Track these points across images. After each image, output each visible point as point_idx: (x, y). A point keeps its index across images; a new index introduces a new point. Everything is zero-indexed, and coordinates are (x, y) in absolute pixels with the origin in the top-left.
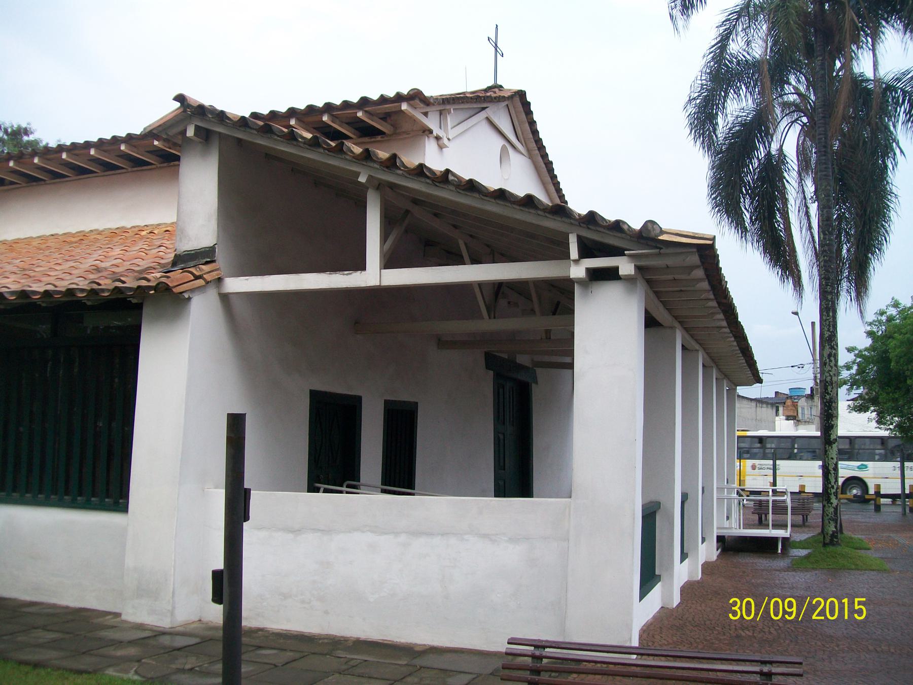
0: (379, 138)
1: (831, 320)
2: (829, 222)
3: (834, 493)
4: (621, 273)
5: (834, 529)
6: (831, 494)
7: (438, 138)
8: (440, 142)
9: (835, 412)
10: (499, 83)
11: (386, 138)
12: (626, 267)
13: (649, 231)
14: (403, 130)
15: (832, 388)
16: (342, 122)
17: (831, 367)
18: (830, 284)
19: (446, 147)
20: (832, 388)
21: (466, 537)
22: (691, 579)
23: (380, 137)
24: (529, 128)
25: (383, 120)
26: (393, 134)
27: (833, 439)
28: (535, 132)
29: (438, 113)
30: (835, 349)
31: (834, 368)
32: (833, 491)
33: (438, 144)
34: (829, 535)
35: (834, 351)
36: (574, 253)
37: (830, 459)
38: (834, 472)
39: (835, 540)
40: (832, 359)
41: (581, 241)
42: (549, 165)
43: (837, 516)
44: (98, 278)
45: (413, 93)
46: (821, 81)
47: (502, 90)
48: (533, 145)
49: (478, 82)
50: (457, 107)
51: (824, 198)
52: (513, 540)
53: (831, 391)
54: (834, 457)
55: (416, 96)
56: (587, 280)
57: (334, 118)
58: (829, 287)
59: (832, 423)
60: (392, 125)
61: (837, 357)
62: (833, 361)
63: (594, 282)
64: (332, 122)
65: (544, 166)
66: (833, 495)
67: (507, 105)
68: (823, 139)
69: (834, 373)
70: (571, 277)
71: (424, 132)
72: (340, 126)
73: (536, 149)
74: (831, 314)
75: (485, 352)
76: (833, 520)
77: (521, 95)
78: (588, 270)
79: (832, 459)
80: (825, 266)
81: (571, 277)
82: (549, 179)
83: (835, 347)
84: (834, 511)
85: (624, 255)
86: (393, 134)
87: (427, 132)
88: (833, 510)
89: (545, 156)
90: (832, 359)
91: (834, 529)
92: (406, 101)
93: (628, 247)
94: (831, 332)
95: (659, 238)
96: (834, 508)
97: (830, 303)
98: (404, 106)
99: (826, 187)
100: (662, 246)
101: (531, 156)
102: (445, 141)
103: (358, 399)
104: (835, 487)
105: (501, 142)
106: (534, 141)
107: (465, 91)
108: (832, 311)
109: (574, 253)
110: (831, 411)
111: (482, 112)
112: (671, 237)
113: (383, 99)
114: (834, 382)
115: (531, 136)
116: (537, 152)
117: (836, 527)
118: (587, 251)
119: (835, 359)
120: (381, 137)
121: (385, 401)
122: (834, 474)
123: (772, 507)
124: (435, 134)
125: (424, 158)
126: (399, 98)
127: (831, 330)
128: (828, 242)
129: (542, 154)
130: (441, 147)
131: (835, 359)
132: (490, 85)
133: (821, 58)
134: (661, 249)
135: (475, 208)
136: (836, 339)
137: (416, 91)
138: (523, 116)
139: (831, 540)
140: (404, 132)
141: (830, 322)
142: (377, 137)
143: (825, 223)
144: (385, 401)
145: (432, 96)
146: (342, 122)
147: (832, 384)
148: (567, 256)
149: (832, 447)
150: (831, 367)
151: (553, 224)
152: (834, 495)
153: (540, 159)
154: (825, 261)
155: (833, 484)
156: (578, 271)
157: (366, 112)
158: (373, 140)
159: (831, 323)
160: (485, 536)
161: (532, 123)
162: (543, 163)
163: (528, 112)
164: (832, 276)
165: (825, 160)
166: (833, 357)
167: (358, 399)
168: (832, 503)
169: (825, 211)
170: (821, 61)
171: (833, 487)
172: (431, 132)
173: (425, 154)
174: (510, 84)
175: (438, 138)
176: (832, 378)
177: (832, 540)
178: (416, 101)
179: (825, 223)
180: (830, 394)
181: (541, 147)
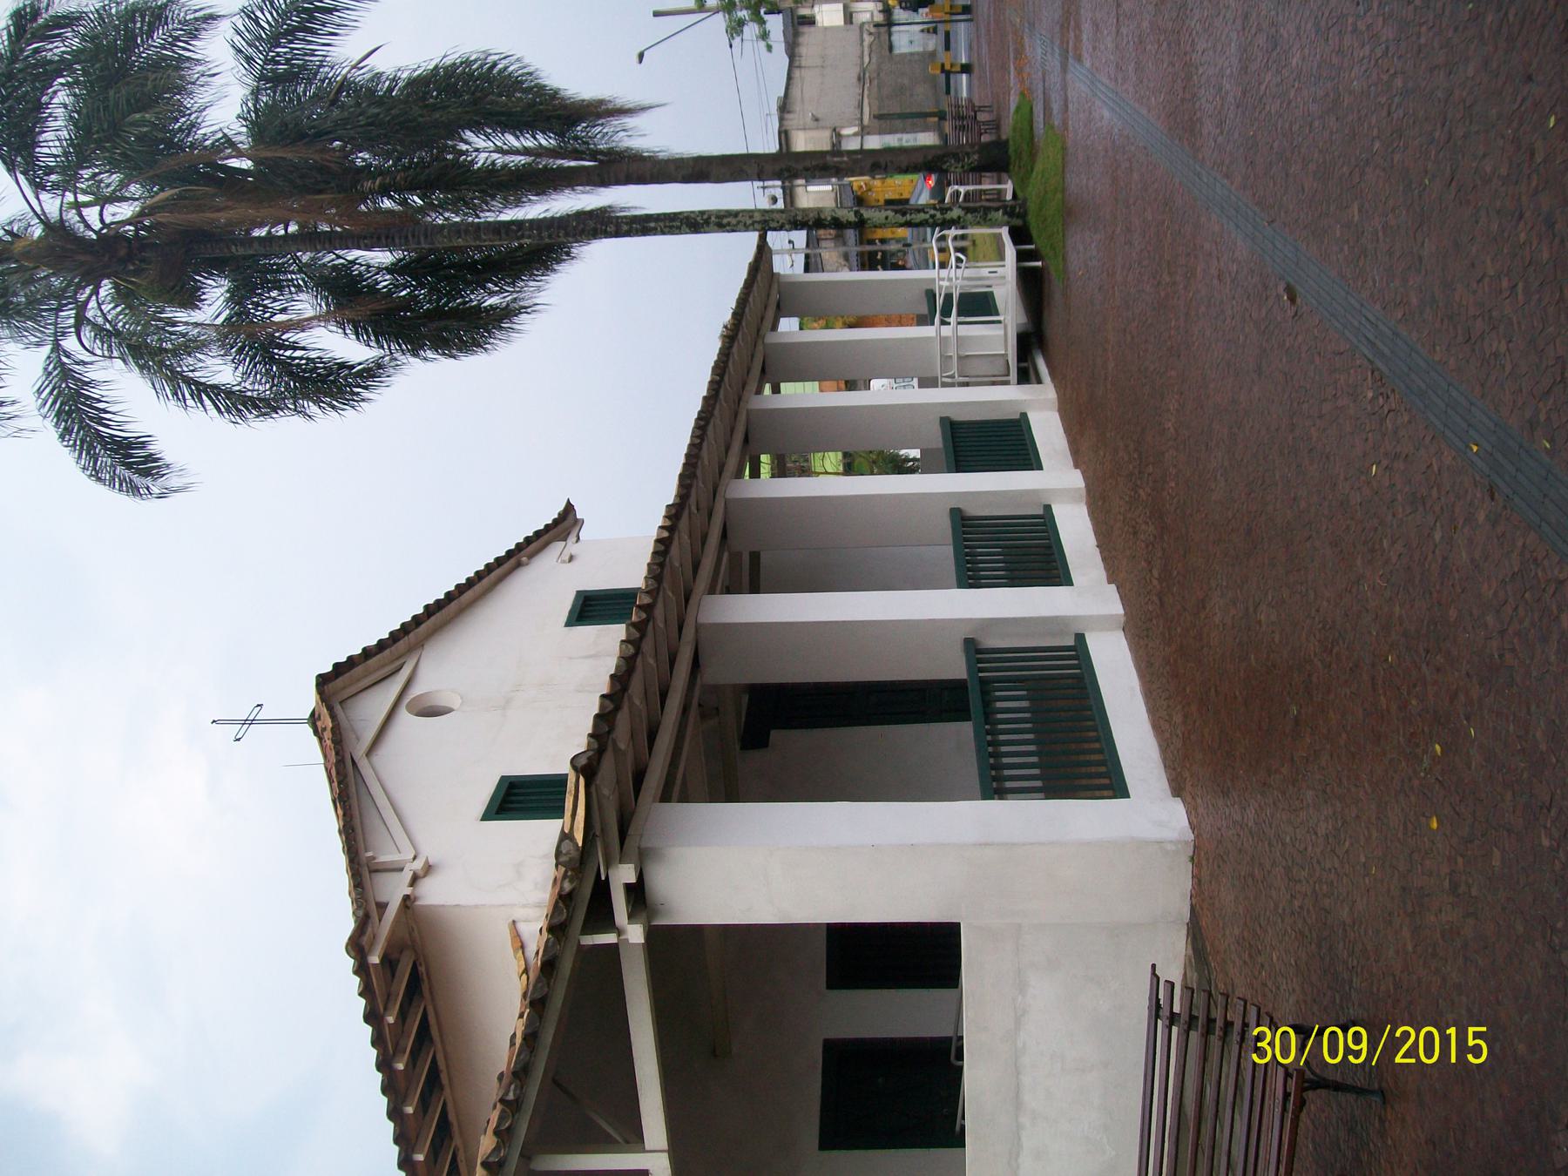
0: (422, 969)
1: (662, 224)
2: (503, 231)
3: (942, 214)
4: (633, 880)
5: (1001, 212)
6: (944, 219)
7: (415, 879)
8: (421, 873)
9: (811, 215)
10: (307, 716)
11: (422, 959)
12: (624, 874)
13: (571, 860)
14: (407, 935)
15: (773, 220)
16: (403, 1032)
17: (739, 222)
18: (604, 228)
19: (427, 861)
20: (773, 220)
21: (1020, 1045)
22: (1085, 499)
23: (420, 968)
24: (374, 658)
25: (397, 965)
26: (415, 951)
27: (856, 216)
28: (382, 645)
29: (373, 875)
30: (709, 218)
31: (739, 218)
32: (938, 215)
33: (424, 876)
34: (1010, 220)
35: (713, 219)
36: (609, 938)
37: (887, 222)
38: (908, 216)
39: (1017, 210)
40: (725, 221)
41: (589, 928)
42: (430, 611)
43: (981, 207)
44: (616, 750)
45: (354, 951)
46: (271, 246)
47: (319, 716)
48: (402, 645)
49: (308, 750)
50: (362, 845)
51: (463, 239)
52: (1022, 987)
53: (778, 222)
54: (884, 216)
55: (357, 946)
56: (644, 915)
57: (398, 1050)
58: (608, 229)
59: (829, 218)
60: (401, 952)
61: (722, 214)
62: (729, 220)
63: (648, 902)
64: (405, 1052)
65: (433, 618)
66: (945, 216)
67: (341, 703)
68: (366, 241)
69: (748, 218)
70: (643, 942)
71: (407, 907)
72: (409, 1037)
73: (406, 638)
74: (652, 225)
75: (741, 749)
76: (986, 214)
77: (323, 681)
78: (631, 917)
79: (887, 218)
80: (574, 236)
81: (643, 942)
82: (453, 604)
83: (705, 217)
84: (972, 213)
85: (607, 877)
86: (415, 951)
87: (408, 903)
88: (969, 216)
89: (417, 620)
90: (725, 221)
91: (1001, 212)
92: (366, 958)
93: (595, 870)
94: (682, 224)
95: (580, 844)
96: (966, 214)
97: (634, 226)
98: (375, 959)
99: (445, 237)
100: (592, 834)
101: (420, 645)
102: (418, 865)
103: (830, 1046)
104: (932, 212)
105: (405, 718)
106: (395, 645)
107: (323, 767)
108: (647, 223)
109: (609, 938)
110: (809, 221)
111: (361, 770)
112: (578, 827)
113: (366, 992)
114: (763, 218)
115: (387, 652)
116: (411, 635)
117: (997, 209)
118: (601, 915)
119: (724, 217)
120: (421, 965)
121: (830, 986)
122: (911, 214)
123: (976, 184)
124: (408, 891)
125: (450, 906)
126: (362, 969)
127: (679, 224)
128: (535, 232)
129: (414, 627)
130: (429, 869)
131: (724, 217)
132: (311, 731)
133: (233, 247)
134: (594, 835)
135: (549, 1058)
136: (692, 215)
137: (349, 947)
138: (358, 670)
139: (1018, 217)
140: (410, 934)
141: (665, 227)
142: (420, 973)
143: (503, 235)
144: (830, 986)
145: (353, 913)
146: (403, 1032)
147: (765, 221)
148: (613, 949)
149: (869, 219)
150: (739, 222)
151: (566, 966)
152: (946, 213)
153: (423, 626)
154: (567, 235)
155: (927, 216)
156: (635, 934)
157: (385, 1009)
158: (425, 978)
159: (667, 224)
160: (1018, 1022)
161: (367, 653)
162: (430, 620)
163: (352, 662)
164: (591, 224)
165: (400, 238)
166: (722, 219)
167: (830, 1046)
168: (959, 217)
169: (484, 237)
170: (238, 247)
171: (933, 216)
172: (406, 898)
173: (443, 906)
174: (308, 700)
175: (415, 879)
176: (756, 222)
177: (1018, 216)
178: (364, 943)
179: (503, 235)
180: (783, 223)
181: (405, 629)
